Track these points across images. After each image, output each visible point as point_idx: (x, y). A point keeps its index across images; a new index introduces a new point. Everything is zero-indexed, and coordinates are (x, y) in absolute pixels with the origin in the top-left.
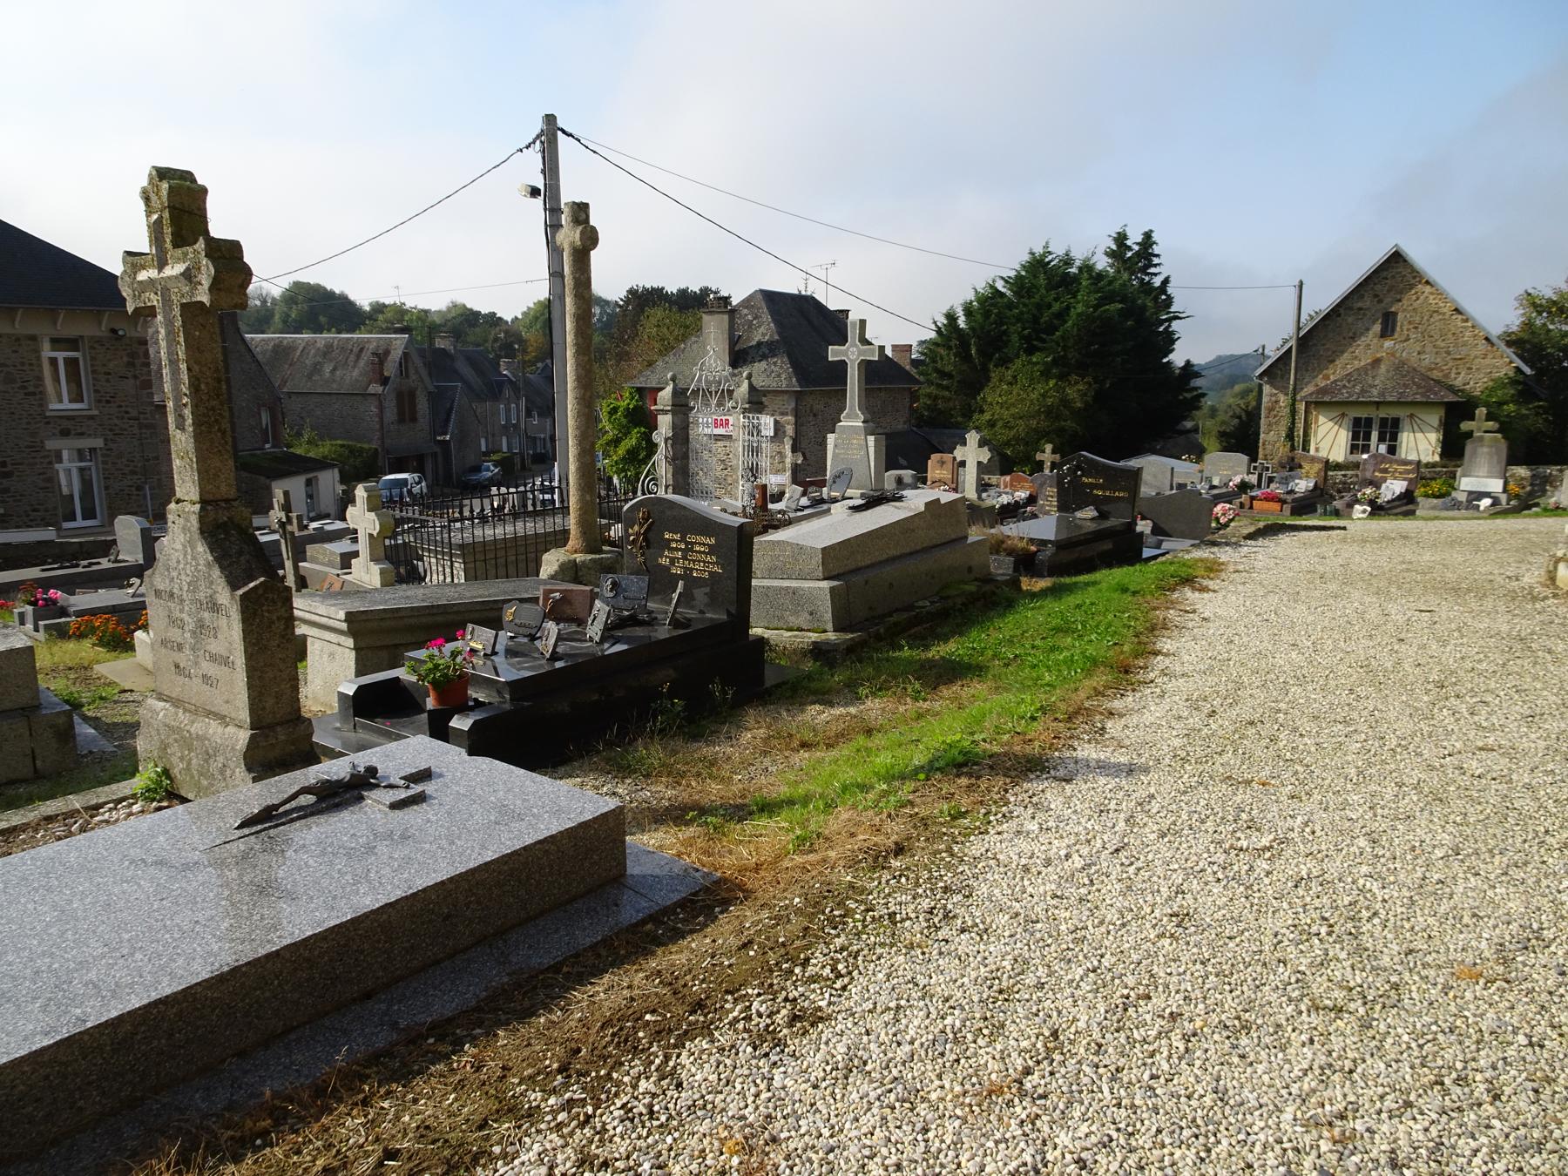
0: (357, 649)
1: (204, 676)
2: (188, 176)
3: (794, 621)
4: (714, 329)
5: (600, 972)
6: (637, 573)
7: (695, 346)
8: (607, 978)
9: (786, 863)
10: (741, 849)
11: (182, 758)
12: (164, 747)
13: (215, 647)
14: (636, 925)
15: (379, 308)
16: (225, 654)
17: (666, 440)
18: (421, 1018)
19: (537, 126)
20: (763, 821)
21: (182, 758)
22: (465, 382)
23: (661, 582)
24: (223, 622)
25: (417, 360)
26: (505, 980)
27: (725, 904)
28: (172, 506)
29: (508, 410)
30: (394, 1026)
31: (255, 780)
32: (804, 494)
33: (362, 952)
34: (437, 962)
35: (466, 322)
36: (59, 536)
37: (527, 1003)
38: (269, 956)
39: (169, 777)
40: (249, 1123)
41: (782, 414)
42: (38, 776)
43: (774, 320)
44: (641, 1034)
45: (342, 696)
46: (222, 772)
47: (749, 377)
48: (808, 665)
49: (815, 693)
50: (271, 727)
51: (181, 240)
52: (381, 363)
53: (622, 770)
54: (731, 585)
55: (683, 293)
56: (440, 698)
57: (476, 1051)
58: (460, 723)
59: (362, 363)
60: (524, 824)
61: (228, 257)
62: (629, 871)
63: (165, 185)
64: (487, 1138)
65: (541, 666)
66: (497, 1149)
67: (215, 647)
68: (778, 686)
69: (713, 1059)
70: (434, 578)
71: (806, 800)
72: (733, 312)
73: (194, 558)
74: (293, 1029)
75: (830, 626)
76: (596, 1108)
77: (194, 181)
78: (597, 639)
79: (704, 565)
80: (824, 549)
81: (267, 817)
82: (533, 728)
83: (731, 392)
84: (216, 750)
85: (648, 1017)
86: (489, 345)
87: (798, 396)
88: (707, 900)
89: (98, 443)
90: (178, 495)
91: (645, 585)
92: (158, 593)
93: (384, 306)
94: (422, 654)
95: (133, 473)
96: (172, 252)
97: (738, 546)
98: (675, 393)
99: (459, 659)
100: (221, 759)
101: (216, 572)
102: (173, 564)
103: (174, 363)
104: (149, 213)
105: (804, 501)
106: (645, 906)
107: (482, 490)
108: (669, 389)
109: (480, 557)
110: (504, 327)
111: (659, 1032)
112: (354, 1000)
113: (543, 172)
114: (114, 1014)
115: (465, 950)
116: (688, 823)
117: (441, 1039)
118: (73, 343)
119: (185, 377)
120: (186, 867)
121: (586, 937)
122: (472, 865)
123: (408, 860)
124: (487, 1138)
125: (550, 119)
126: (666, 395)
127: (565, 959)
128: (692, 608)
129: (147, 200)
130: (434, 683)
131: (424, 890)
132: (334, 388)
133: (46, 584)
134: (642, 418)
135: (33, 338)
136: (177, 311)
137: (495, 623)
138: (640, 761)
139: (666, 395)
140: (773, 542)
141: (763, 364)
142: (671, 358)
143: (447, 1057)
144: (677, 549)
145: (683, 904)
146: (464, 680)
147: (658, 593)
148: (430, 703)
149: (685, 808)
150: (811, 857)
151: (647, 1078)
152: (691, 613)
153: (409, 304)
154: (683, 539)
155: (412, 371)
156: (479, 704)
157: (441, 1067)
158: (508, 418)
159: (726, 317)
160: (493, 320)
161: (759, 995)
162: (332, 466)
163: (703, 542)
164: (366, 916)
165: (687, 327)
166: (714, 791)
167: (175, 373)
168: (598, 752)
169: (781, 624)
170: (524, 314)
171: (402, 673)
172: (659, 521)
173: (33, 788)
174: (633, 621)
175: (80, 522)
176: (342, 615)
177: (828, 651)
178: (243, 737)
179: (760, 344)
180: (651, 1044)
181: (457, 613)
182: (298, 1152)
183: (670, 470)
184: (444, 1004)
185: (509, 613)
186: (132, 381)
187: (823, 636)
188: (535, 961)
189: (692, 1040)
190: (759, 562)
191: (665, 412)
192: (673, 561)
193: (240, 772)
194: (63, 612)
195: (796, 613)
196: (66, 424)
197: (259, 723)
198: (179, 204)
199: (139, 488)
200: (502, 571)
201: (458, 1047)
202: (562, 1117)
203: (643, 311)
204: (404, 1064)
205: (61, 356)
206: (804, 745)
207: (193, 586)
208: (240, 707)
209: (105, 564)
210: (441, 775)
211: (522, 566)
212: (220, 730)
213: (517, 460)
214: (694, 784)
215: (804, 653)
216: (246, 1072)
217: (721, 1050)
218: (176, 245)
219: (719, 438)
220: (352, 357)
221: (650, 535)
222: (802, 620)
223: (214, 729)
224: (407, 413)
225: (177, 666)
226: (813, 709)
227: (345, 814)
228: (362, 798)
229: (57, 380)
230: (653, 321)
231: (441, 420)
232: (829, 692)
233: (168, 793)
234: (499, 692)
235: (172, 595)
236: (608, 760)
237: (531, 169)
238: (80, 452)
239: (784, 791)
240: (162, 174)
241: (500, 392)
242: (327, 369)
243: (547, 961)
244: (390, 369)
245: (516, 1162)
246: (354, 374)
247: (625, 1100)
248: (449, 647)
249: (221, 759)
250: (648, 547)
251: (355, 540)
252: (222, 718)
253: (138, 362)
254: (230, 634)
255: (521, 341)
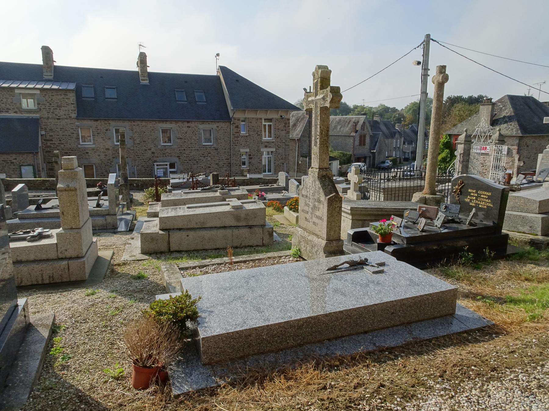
0: (352, 219)
1: (314, 222)
2: (326, 67)
3: (521, 229)
4: (485, 112)
5: (448, 346)
6: (455, 203)
7: (475, 118)
8: (449, 349)
9: (525, 325)
10: (500, 315)
11: (304, 246)
12: (300, 242)
13: (318, 213)
14: (460, 333)
15: (356, 107)
16: (321, 216)
17: (460, 154)
18: (383, 344)
19: (423, 38)
20: (512, 306)
21: (304, 246)
22: (383, 132)
23: (465, 208)
24: (321, 206)
25: (367, 124)
26: (411, 339)
27: (498, 334)
28: (310, 169)
29: (397, 142)
30: (374, 344)
31: (326, 257)
32: (525, 178)
33: (366, 318)
34: (388, 327)
35: (385, 111)
36: (7, 177)
37: (420, 350)
38: (340, 312)
39: (300, 251)
40: (333, 362)
41: (512, 145)
42: (263, 245)
43: (513, 107)
44: (471, 373)
45: (349, 234)
46: (316, 252)
47: (500, 130)
48: (528, 248)
49: (531, 259)
50: (332, 241)
51: (322, 88)
52: (356, 126)
53: (447, 276)
54: (496, 212)
55: (470, 98)
56: (383, 239)
57: (403, 361)
58: (390, 249)
59: (350, 125)
60: (419, 288)
61: (336, 92)
62: (456, 313)
63: (320, 71)
64: (415, 391)
65: (417, 234)
66: (419, 396)
67: (318, 213)
68: (514, 254)
69: (503, 391)
70: (373, 198)
71: (532, 302)
72: (494, 104)
73: (315, 186)
74: (344, 336)
75: (540, 233)
76: (456, 393)
77: (328, 69)
78: (439, 226)
79: (485, 202)
80: (540, 202)
81: (335, 268)
82: (421, 253)
83: (490, 136)
84: (315, 245)
85: (473, 367)
86: (392, 119)
87: (521, 138)
88: (489, 331)
89: (274, 150)
90: (312, 166)
91: (459, 208)
92: (303, 196)
93: (358, 106)
94: (377, 224)
95: (282, 159)
96: (320, 91)
97: (502, 198)
98: (466, 136)
99: (390, 227)
100: (316, 248)
101: (321, 190)
102: (308, 187)
103: (316, 125)
104: (314, 80)
105: (524, 181)
106: (463, 328)
107: (387, 169)
108: (464, 135)
109: (390, 193)
110: (398, 112)
111: (479, 374)
112: (362, 333)
113: (423, 55)
114: (299, 318)
115: (397, 326)
116: (478, 300)
117: (390, 353)
118: (270, 120)
119: (319, 130)
120: (313, 279)
121: (441, 332)
122: (402, 298)
123: (380, 292)
124: (415, 391)
125: (428, 36)
126: (462, 138)
127: (433, 338)
128: (477, 219)
129: (314, 76)
130: (381, 234)
131: (386, 302)
132: (340, 134)
133: (261, 190)
134: (450, 147)
135: (261, 119)
136: (319, 110)
137: (401, 216)
138: (455, 273)
139: (462, 138)
140: (515, 197)
141: (505, 125)
142: (464, 123)
143: (393, 360)
144: (473, 196)
145: (479, 330)
146: (391, 235)
147: (463, 212)
148: (379, 241)
149: (477, 295)
150: (539, 325)
151: (476, 390)
152: (477, 221)
153: (366, 105)
154: (476, 192)
155: (365, 128)
156: (395, 244)
157: (391, 362)
158: (396, 145)
159: (490, 107)
160: (394, 110)
161: (522, 373)
162: (337, 159)
163: (485, 194)
164: (368, 306)
165: (471, 111)
166: (488, 291)
167: (316, 128)
168: (438, 267)
169: (515, 230)
170: (406, 108)
171: (367, 229)
172: (465, 186)
173: (263, 249)
174: (453, 221)
175: (267, 173)
176: (349, 208)
177: (538, 243)
178: (324, 242)
179: (504, 117)
180: (476, 377)
181: (386, 211)
182: (348, 375)
183: (461, 166)
184: (391, 342)
185: (406, 213)
186: (284, 131)
187: (536, 237)
188: (422, 336)
189: (494, 381)
190: (509, 204)
191: (462, 144)
192: (471, 200)
193: (322, 254)
194: (265, 199)
195: (523, 226)
196: (266, 144)
197: (329, 240)
198: (323, 78)
199: (283, 164)
200: (397, 198)
201: (396, 357)
202: (442, 393)
203: (453, 105)
204: (378, 358)
205: (267, 124)
206: (527, 279)
207: (314, 194)
208: (324, 233)
209: (275, 186)
210: (388, 265)
211: (404, 197)
212: (317, 239)
213: (398, 160)
214: (478, 286)
215: (526, 243)
216: (331, 346)
217: (507, 389)
218: (321, 89)
219: (483, 154)
220: (347, 124)
221: (462, 190)
222: (526, 229)
223: (315, 239)
224: (362, 142)
225: (306, 218)
226: (530, 266)
227: (358, 272)
228: (363, 268)
229: (265, 131)
230: (457, 109)
231: (373, 145)
232: (537, 260)
233: (300, 257)
234: (402, 240)
235: (307, 196)
236: (441, 271)
237: (419, 55)
238: (268, 152)
239: (521, 296)
240: (319, 67)
241: (395, 135)
242: (339, 127)
243: (426, 337)
244: (359, 128)
245: (427, 402)
246: (347, 130)
247: (467, 394)
248: (387, 222)
249: (316, 248)
250: (461, 194)
251: (350, 184)
252: (317, 236)
253: (287, 126)
254: (323, 210)
255: (404, 117)
